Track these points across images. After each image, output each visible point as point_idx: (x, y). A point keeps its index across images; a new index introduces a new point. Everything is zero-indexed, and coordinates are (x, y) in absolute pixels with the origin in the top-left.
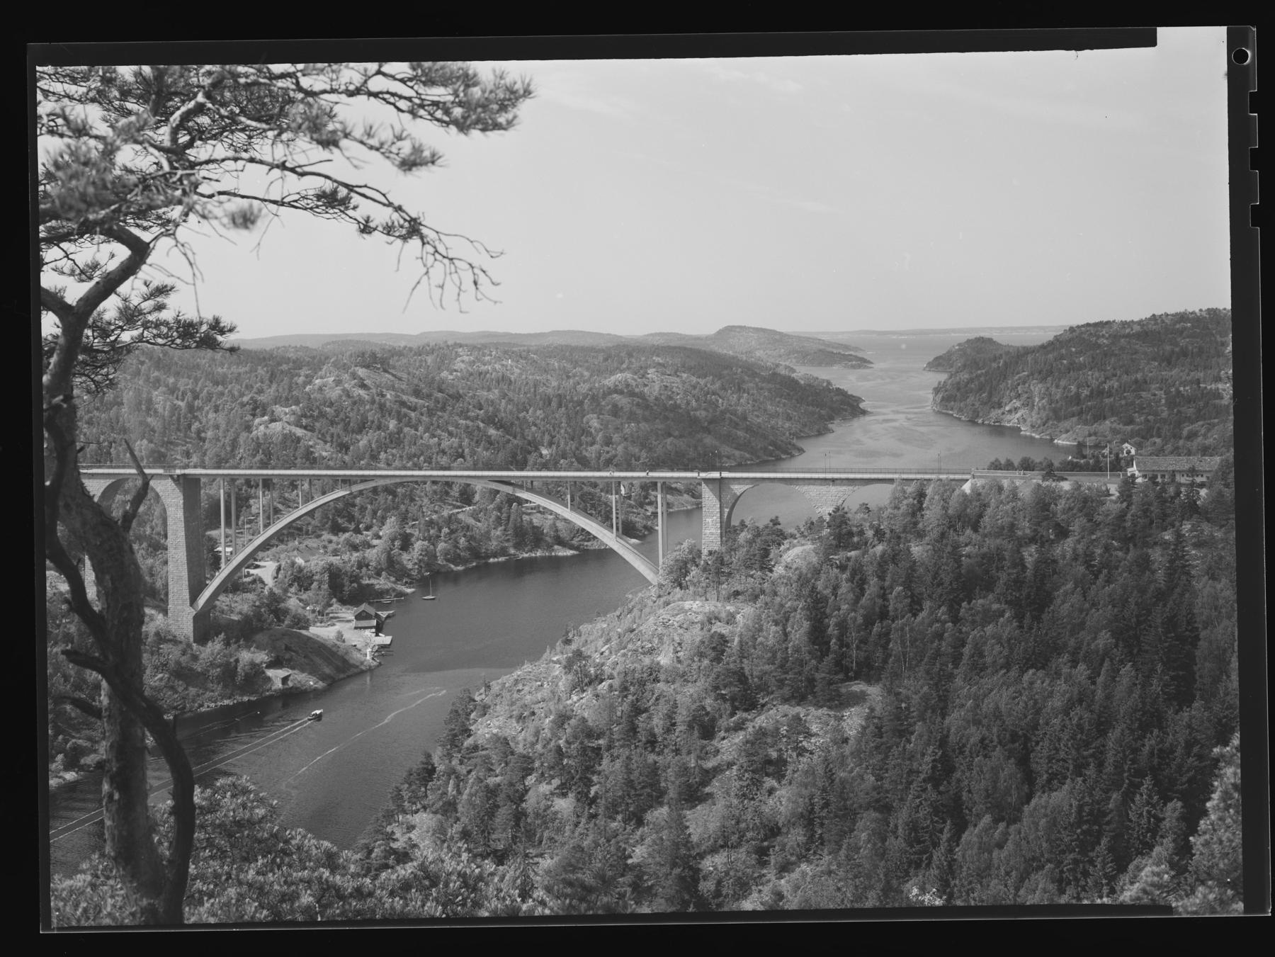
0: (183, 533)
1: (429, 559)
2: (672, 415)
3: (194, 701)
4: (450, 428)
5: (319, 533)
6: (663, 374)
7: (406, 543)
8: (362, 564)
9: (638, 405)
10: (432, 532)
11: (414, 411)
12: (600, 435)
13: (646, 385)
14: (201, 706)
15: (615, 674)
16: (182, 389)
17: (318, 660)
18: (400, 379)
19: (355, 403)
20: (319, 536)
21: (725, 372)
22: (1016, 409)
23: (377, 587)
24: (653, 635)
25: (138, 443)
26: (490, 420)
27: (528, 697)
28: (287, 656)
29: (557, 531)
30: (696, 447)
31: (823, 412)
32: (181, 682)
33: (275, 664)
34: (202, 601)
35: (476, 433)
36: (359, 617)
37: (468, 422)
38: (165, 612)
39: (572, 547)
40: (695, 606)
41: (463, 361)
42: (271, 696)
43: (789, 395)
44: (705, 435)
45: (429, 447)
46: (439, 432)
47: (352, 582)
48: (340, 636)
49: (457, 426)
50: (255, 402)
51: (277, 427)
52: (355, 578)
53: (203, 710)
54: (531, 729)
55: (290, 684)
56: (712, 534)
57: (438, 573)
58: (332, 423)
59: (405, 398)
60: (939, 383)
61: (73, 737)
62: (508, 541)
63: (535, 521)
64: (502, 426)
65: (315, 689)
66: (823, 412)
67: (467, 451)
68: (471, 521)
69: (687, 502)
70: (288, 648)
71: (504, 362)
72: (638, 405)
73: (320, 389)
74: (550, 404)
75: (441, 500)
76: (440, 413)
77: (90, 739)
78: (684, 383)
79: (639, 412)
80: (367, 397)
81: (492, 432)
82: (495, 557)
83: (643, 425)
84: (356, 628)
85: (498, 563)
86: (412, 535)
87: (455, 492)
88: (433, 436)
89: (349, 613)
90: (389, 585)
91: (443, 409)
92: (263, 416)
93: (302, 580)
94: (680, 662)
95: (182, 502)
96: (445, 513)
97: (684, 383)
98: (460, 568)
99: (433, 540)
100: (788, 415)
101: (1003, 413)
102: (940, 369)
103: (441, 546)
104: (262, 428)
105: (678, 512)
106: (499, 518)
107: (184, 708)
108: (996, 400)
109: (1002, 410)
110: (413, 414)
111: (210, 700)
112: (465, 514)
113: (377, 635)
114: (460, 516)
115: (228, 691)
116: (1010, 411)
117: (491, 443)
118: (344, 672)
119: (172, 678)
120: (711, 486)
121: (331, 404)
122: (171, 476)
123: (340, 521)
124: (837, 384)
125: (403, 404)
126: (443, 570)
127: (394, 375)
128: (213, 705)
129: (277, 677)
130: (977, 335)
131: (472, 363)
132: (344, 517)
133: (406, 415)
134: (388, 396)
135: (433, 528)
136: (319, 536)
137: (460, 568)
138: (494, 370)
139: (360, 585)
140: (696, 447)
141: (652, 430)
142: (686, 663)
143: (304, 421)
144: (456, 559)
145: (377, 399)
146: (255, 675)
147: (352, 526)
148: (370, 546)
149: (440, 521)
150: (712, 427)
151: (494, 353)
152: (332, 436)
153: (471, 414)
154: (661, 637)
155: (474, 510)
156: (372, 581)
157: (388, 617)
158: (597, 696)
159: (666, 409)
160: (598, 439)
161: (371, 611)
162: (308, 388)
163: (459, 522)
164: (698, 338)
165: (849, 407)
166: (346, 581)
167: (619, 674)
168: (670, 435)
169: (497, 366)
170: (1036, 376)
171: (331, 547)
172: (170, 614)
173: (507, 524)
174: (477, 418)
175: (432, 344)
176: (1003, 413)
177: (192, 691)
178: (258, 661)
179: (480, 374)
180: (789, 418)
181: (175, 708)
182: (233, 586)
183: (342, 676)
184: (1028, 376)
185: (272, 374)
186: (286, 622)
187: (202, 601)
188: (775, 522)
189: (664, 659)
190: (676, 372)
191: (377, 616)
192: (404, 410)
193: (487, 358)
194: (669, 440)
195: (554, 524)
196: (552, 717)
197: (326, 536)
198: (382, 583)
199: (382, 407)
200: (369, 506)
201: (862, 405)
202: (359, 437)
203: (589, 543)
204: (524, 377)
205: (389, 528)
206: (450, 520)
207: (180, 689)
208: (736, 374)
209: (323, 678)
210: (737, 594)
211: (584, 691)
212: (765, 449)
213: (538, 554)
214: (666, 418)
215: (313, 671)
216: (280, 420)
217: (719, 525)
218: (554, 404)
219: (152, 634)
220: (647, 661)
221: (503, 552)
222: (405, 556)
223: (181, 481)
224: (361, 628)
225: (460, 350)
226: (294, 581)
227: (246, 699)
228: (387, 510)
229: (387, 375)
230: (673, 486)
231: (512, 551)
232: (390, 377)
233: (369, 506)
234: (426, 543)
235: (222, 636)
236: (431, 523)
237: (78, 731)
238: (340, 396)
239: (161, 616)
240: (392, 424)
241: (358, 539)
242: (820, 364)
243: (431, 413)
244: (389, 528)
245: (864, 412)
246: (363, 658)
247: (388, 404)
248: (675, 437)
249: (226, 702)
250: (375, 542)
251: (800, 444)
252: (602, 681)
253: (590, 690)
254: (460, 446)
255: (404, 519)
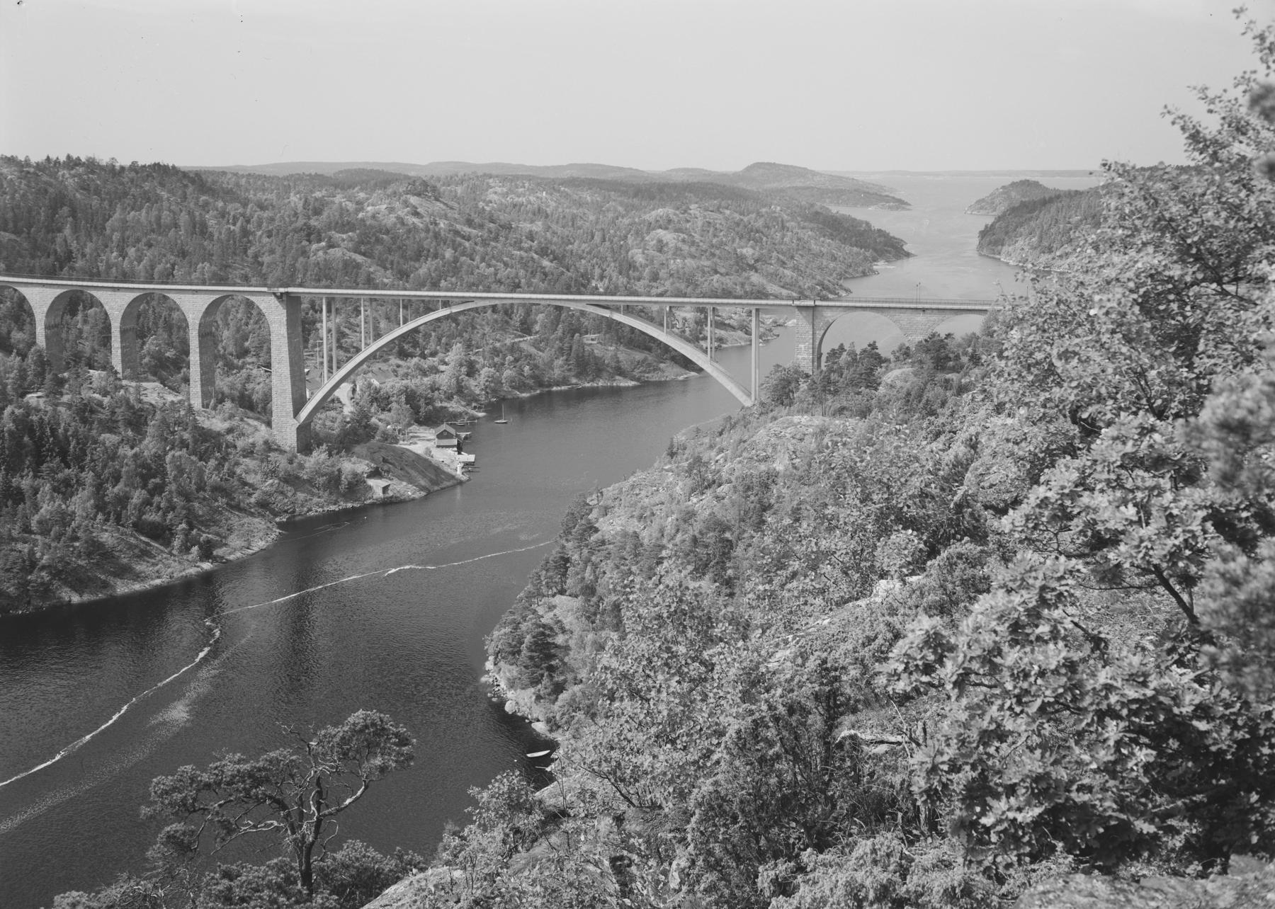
0: (287, 349)
1: (493, 387)
2: (717, 252)
3: (302, 506)
4: (505, 259)
5: (386, 357)
6: (706, 210)
7: (472, 371)
8: (434, 388)
9: (683, 241)
10: (496, 359)
11: (468, 240)
12: (647, 270)
13: (688, 221)
14: (310, 510)
15: (733, 479)
16: (232, 213)
17: (414, 473)
18: (452, 208)
19: (409, 231)
20: (386, 361)
21: (764, 210)
22: (1067, 254)
23: (451, 410)
24: (767, 446)
25: (200, 265)
26: (543, 252)
27: (647, 500)
28: (385, 468)
29: (618, 362)
30: (743, 285)
31: (868, 254)
32: (289, 488)
33: (376, 474)
34: (304, 414)
35: (530, 264)
36: (440, 436)
37: (522, 253)
38: (269, 424)
39: (633, 379)
40: (803, 420)
41: (496, 193)
42: (373, 505)
43: (831, 235)
44: (752, 273)
45: (487, 277)
46: (494, 262)
47: (427, 404)
48: (428, 451)
49: (511, 256)
50: (309, 227)
51: (336, 253)
52: (430, 401)
53: (311, 514)
54: (655, 526)
55: (390, 493)
56: (804, 359)
57: (504, 399)
58: (390, 251)
59: (458, 227)
60: (986, 226)
61: (204, 532)
62: (570, 370)
63: (596, 351)
64: (555, 259)
65: (413, 499)
66: (868, 254)
67: (523, 281)
68: (533, 350)
69: (741, 338)
70: (385, 461)
71: (538, 195)
72: (683, 241)
73: (374, 217)
74: (593, 237)
75: (504, 329)
76: (493, 244)
77: (218, 534)
78: (727, 219)
79: (685, 248)
80: (421, 225)
81: (546, 263)
82: (558, 385)
83: (689, 261)
84: (438, 447)
85: (561, 391)
86: (475, 362)
87: (517, 319)
88: (489, 266)
89: (430, 433)
90: (461, 409)
91: (496, 239)
92: (319, 241)
93: (381, 400)
94: (795, 468)
95: (285, 319)
96: (508, 342)
97: (727, 219)
98: (525, 395)
99: (499, 367)
100: (833, 255)
101: (1054, 259)
102: (982, 212)
103: (508, 373)
104: (321, 253)
105: (732, 347)
106: (561, 349)
107: (294, 512)
108: (1047, 244)
109: (1053, 255)
110: (467, 244)
111: (317, 504)
112: (526, 343)
113: (459, 453)
114: (522, 345)
115: (334, 498)
116: (1061, 257)
117: (545, 274)
118: (437, 484)
119: (282, 484)
120: (804, 313)
121: (388, 232)
122: (274, 294)
123: (406, 347)
124: (876, 225)
125: (457, 233)
126: (509, 397)
127: (445, 204)
128: (321, 510)
129: (377, 486)
130: (1023, 178)
131: (505, 195)
132: (409, 343)
133: (460, 244)
134: (442, 225)
135: (498, 356)
136: (386, 361)
137: (525, 395)
138: (529, 202)
139: (435, 408)
140: (743, 285)
141: (698, 268)
142: (801, 470)
143: (363, 248)
144: (522, 387)
145: (431, 227)
146: (356, 486)
147: (418, 351)
148: (438, 371)
149: (503, 349)
150: (759, 265)
151: (527, 185)
152: (392, 263)
153: (525, 245)
154: (774, 447)
155: (536, 340)
156: (445, 404)
157: (466, 438)
158: (717, 497)
159: (712, 246)
160: (645, 274)
161: (452, 431)
162: (360, 215)
163: (521, 351)
164: (724, 175)
165: (892, 249)
166: (422, 403)
167: (737, 478)
168: (716, 272)
169: (532, 199)
170: (1089, 221)
171: (401, 371)
172: (273, 426)
173: (569, 355)
174: (530, 249)
175: (461, 174)
176: (1054, 259)
177: (301, 496)
178: (359, 471)
179: (515, 206)
180: (834, 258)
181: (286, 511)
182: (324, 404)
183: (436, 488)
184: (1081, 220)
185: (306, 201)
186: (377, 438)
187: (304, 414)
188: (873, 346)
189: (779, 466)
190: (718, 208)
191: (457, 436)
192: (459, 239)
193: (521, 190)
194: (716, 277)
195: (616, 355)
196: (674, 517)
197: (394, 361)
198: (455, 406)
199: (437, 236)
200: (433, 334)
201: (905, 248)
202: (417, 265)
203: (649, 375)
204: (560, 210)
205: (456, 353)
206: (513, 349)
207: (289, 494)
208: (775, 212)
209: (422, 488)
210: (841, 410)
211: (703, 494)
212: (812, 289)
213: (600, 384)
214: (713, 255)
215: (411, 481)
216: (339, 246)
217: (811, 351)
218: (597, 238)
219: (261, 442)
220: (763, 467)
221: (565, 381)
222: (472, 383)
223: (284, 298)
224: (443, 447)
225: (491, 181)
226: (372, 402)
227: (349, 505)
228: (452, 337)
229: (438, 204)
230: (727, 322)
231: (574, 381)
232: (442, 205)
233: (433, 334)
234: (492, 370)
235: (324, 447)
236: (496, 352)
237: (207, 526)
238: (395, 224)
239: (263, 427)
240: (449, 254)
241: (426, 364)
242: (855, 205)
243: (485, 243)
244: (456, 353)
245: (908, 255)
246: (453, 473)
247: (442, 233)
248: (721, 274)
249: (332, 508)
250: (442, 368)
251: (847, 284)
252: (720, 485)
253: (709, 492)
254: (517, 276)
255: (469, 346)
